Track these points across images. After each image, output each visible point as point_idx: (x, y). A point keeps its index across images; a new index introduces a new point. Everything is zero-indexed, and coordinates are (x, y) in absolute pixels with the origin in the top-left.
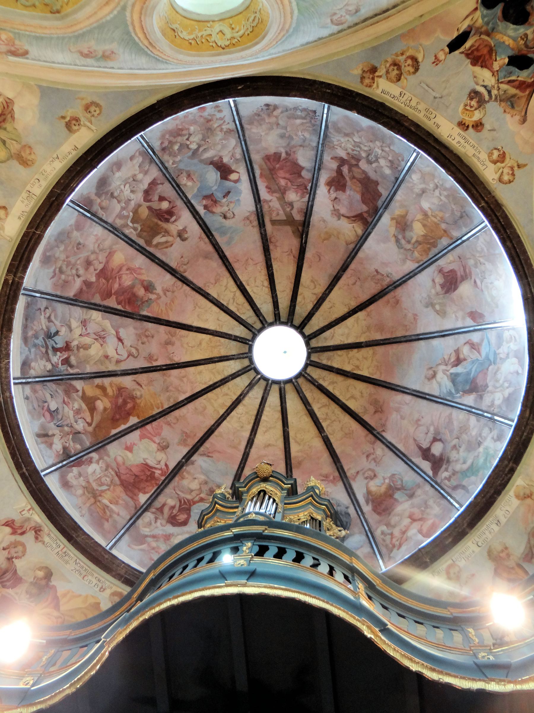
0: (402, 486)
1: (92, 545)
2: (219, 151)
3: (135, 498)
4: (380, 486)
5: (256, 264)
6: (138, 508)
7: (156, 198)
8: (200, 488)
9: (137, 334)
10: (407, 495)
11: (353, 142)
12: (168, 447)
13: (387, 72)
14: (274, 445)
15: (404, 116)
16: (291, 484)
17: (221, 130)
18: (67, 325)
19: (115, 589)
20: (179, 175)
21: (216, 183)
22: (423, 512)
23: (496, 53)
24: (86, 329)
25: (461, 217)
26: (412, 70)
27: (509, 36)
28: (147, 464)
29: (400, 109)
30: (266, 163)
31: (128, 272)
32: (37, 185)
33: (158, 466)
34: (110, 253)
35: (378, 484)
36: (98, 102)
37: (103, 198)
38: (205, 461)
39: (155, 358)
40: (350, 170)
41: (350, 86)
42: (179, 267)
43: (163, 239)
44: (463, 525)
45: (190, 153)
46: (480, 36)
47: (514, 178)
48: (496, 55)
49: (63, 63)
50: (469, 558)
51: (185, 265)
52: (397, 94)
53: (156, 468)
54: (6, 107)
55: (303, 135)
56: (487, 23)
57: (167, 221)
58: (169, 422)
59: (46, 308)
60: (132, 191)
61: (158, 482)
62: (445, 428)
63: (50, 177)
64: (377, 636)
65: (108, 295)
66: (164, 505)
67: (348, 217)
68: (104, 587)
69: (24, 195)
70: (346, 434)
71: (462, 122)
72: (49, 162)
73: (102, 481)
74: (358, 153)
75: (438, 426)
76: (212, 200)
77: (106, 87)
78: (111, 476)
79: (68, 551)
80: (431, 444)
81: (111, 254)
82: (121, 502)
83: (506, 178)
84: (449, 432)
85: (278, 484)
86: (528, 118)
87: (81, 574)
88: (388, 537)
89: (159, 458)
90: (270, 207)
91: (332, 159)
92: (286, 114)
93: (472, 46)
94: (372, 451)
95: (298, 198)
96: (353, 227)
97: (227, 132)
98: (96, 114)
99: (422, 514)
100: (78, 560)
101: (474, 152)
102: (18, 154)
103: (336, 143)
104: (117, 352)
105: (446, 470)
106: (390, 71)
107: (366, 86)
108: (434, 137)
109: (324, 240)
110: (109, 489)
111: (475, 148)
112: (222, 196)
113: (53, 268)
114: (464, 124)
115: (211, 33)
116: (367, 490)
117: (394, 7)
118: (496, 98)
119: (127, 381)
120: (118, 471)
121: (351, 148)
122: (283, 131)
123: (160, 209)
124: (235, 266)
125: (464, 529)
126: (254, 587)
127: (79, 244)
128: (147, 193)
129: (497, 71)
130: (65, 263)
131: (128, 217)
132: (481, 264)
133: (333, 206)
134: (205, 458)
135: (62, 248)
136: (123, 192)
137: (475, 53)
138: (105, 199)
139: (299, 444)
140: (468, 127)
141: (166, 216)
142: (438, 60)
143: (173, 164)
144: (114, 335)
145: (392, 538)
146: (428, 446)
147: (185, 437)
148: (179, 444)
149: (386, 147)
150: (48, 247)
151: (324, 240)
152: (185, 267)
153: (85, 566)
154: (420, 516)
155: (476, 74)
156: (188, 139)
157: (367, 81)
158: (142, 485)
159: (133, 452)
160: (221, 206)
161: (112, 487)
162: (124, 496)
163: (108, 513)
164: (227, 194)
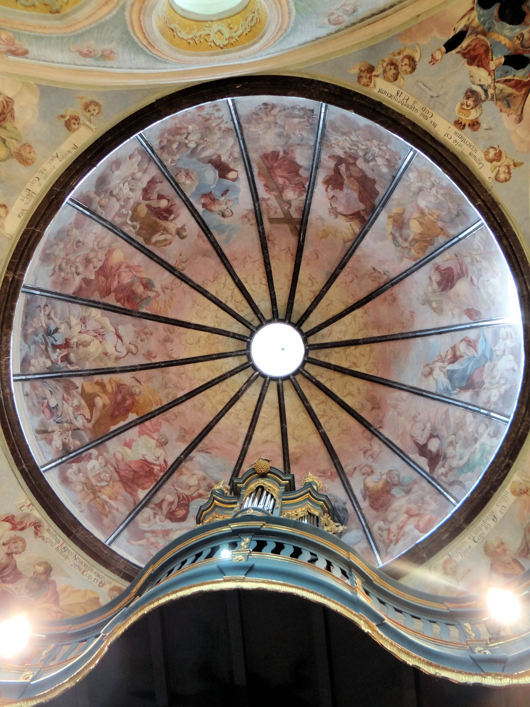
0: (399, 481)
1: (91, 540)
2: (218, 150)
3: (134, 493)
4: (378, 482)
5: (254, 262)
6: (137, 504)
7: (155, 196)
8: (199, 484)
9: (136, 331)
10: (403, 490)
11: (350, 141)
12: (167, 443)
13: (385, 72)
14: (272, 442)
15: (401, 115)
16: (289, 480)
17: (220, 129)
18: (66, 322)
19: (114, 584)
20: (177, 174)
21: (214, 182)
22: (420, 508)
23: (492, 53)
24: (85, 326)
25: (458, 215)
26: (409, 69)
27: (505, 36)
28: (145, 461)
29: (397, 108)
30: (264, 162)
31: (127, 270)
32: (37, 183)
33: (157, 462)
34: (109, 251)
35: (375, 480)
36: (97, 101)
37: (102, 196)
38: (203, 457)
39: (154, 355)
40: (347, 169)
41: (348, 86)
42: (178, 265)
43: (162, 237)
44: (460, 521)
45: (189, 152)
46: (476, 36)
47: (510, 177)
48: (492, 55)
49: (62, 63)
50: (466, 554)
51: (183, 262)
52: (394, 93)
53: (154, 464)
54: (6, 106)
55: (301, 134)
56: (484, 23)
57: (166, 219)
58: (167, 418)
59: (46, 305)
60: (131, 190)
61: (156, 478)
62: (442, 425)
63: (50, 176)
64: (374, 630)
65: (107, 292)
66: (163, 501)
67: (345, 216)
68: (103, 582)
69: (24, 193)
70: (343, 430)
71: (458, 121)
72: (48, 161)
73: (102, 477)
74: (355, 151)
75: (434, 423)
76: (210, 199)
77: (105, 87)
78: (110, 472)
79: (67, 546)
80: (428, 441)
81: (110, 252)
82: (120, 498)
83: (502, 176)
84: (446, 428)
85: (276, 480)
86: (524, 117)
87: (80, 569)
88: (385, 533)
89: (158, 454)
90: (268, 205)
91: (329, 157)
92: (284, 113)
93: (469, 46)
94: (370, 447)
95: (296, 197)
96: (351, 225)
97: (225, 130)
98: (95, 113)
99: (419, 510)
100: (77, 556)
101: (471, 151)
102: (18, 153)
103: (333, 142)
104: (116, 349)
105: (443, 466)
106: (387, 70)
107: (364, 85)
108: (431, 136)
109: (322, 238)
110: (108, 485)
111: (471, 147)
112: (221, 194)
113: (53, 266)
114: (461, 123)
115: (209, 33)
116: (364, 486)
117: (391, 7)
118: (492, 97)
119: (126, 378)
120: (117, 467)
121: (348, 147)
122: (281, 130)
123: (159, 207)
124: (234, 264)
125: (461, 524)
126: (252, 582)
127: (79, 242)
128: (146, 191)
129: (494, 70)
130: (65, 261)
131: (127, 215)
132: (477, 261)
133: (331, 205)
134: (204, 454)
135: (62, 246)
136: (122, 190)
137: (472, 52)
138: (104, 198)
139: (297, 441)
140: (464, 125)
141: (165, 215)
142: (435, 60)
143: (171, 162)
144: (113, 332)
145: (389, 534)
146: (425, 442)
147: (183, 434)
148: (178, 440)
149: (383, 145)
150: (48, 245)
151: (322, 238)
152: (183, 265)
153: (84, 561)
154: (417, 512)
155: (472, 74)
156: (186, 138)
157: (364, 80)
158: (141, 481)
159: (132, 448)
160: (219, 204)
161: (111, 483)
162: (123, 492)
163: (107, 509)
164: (225, 192)
